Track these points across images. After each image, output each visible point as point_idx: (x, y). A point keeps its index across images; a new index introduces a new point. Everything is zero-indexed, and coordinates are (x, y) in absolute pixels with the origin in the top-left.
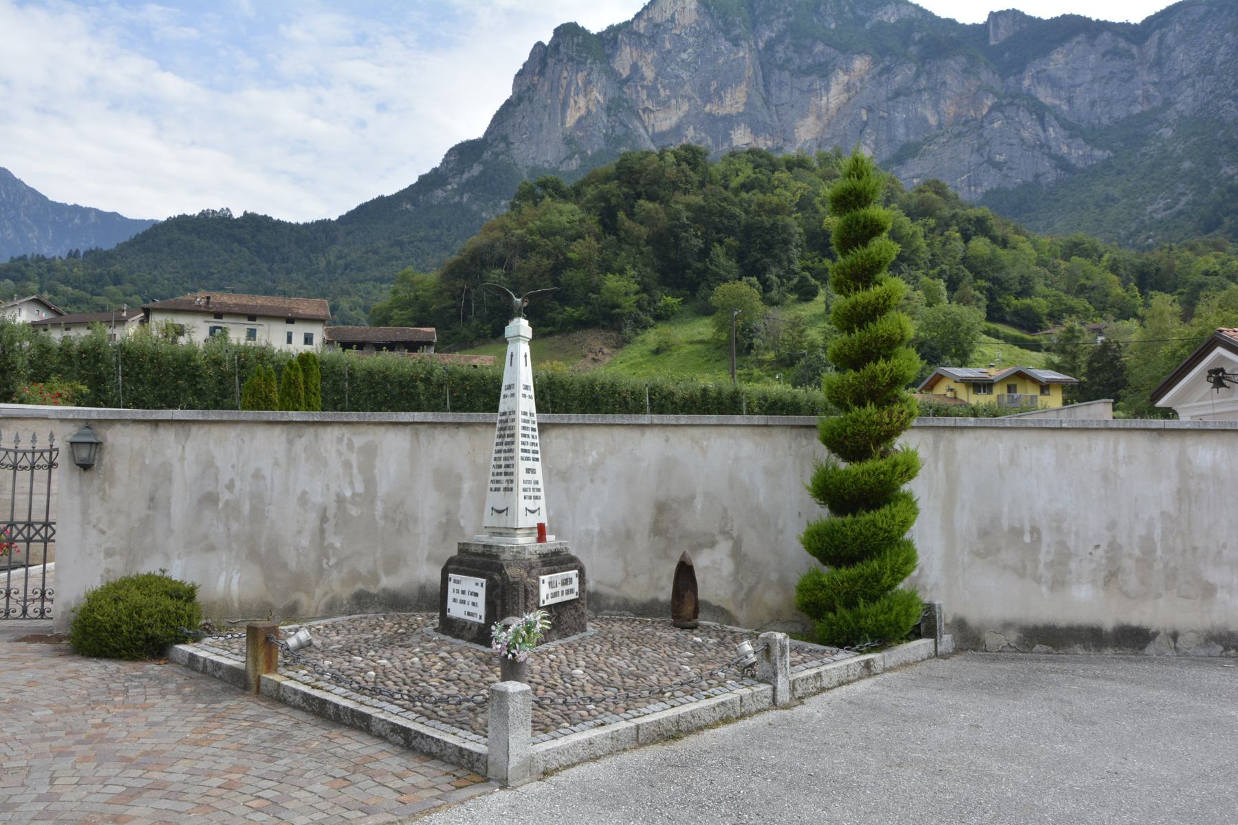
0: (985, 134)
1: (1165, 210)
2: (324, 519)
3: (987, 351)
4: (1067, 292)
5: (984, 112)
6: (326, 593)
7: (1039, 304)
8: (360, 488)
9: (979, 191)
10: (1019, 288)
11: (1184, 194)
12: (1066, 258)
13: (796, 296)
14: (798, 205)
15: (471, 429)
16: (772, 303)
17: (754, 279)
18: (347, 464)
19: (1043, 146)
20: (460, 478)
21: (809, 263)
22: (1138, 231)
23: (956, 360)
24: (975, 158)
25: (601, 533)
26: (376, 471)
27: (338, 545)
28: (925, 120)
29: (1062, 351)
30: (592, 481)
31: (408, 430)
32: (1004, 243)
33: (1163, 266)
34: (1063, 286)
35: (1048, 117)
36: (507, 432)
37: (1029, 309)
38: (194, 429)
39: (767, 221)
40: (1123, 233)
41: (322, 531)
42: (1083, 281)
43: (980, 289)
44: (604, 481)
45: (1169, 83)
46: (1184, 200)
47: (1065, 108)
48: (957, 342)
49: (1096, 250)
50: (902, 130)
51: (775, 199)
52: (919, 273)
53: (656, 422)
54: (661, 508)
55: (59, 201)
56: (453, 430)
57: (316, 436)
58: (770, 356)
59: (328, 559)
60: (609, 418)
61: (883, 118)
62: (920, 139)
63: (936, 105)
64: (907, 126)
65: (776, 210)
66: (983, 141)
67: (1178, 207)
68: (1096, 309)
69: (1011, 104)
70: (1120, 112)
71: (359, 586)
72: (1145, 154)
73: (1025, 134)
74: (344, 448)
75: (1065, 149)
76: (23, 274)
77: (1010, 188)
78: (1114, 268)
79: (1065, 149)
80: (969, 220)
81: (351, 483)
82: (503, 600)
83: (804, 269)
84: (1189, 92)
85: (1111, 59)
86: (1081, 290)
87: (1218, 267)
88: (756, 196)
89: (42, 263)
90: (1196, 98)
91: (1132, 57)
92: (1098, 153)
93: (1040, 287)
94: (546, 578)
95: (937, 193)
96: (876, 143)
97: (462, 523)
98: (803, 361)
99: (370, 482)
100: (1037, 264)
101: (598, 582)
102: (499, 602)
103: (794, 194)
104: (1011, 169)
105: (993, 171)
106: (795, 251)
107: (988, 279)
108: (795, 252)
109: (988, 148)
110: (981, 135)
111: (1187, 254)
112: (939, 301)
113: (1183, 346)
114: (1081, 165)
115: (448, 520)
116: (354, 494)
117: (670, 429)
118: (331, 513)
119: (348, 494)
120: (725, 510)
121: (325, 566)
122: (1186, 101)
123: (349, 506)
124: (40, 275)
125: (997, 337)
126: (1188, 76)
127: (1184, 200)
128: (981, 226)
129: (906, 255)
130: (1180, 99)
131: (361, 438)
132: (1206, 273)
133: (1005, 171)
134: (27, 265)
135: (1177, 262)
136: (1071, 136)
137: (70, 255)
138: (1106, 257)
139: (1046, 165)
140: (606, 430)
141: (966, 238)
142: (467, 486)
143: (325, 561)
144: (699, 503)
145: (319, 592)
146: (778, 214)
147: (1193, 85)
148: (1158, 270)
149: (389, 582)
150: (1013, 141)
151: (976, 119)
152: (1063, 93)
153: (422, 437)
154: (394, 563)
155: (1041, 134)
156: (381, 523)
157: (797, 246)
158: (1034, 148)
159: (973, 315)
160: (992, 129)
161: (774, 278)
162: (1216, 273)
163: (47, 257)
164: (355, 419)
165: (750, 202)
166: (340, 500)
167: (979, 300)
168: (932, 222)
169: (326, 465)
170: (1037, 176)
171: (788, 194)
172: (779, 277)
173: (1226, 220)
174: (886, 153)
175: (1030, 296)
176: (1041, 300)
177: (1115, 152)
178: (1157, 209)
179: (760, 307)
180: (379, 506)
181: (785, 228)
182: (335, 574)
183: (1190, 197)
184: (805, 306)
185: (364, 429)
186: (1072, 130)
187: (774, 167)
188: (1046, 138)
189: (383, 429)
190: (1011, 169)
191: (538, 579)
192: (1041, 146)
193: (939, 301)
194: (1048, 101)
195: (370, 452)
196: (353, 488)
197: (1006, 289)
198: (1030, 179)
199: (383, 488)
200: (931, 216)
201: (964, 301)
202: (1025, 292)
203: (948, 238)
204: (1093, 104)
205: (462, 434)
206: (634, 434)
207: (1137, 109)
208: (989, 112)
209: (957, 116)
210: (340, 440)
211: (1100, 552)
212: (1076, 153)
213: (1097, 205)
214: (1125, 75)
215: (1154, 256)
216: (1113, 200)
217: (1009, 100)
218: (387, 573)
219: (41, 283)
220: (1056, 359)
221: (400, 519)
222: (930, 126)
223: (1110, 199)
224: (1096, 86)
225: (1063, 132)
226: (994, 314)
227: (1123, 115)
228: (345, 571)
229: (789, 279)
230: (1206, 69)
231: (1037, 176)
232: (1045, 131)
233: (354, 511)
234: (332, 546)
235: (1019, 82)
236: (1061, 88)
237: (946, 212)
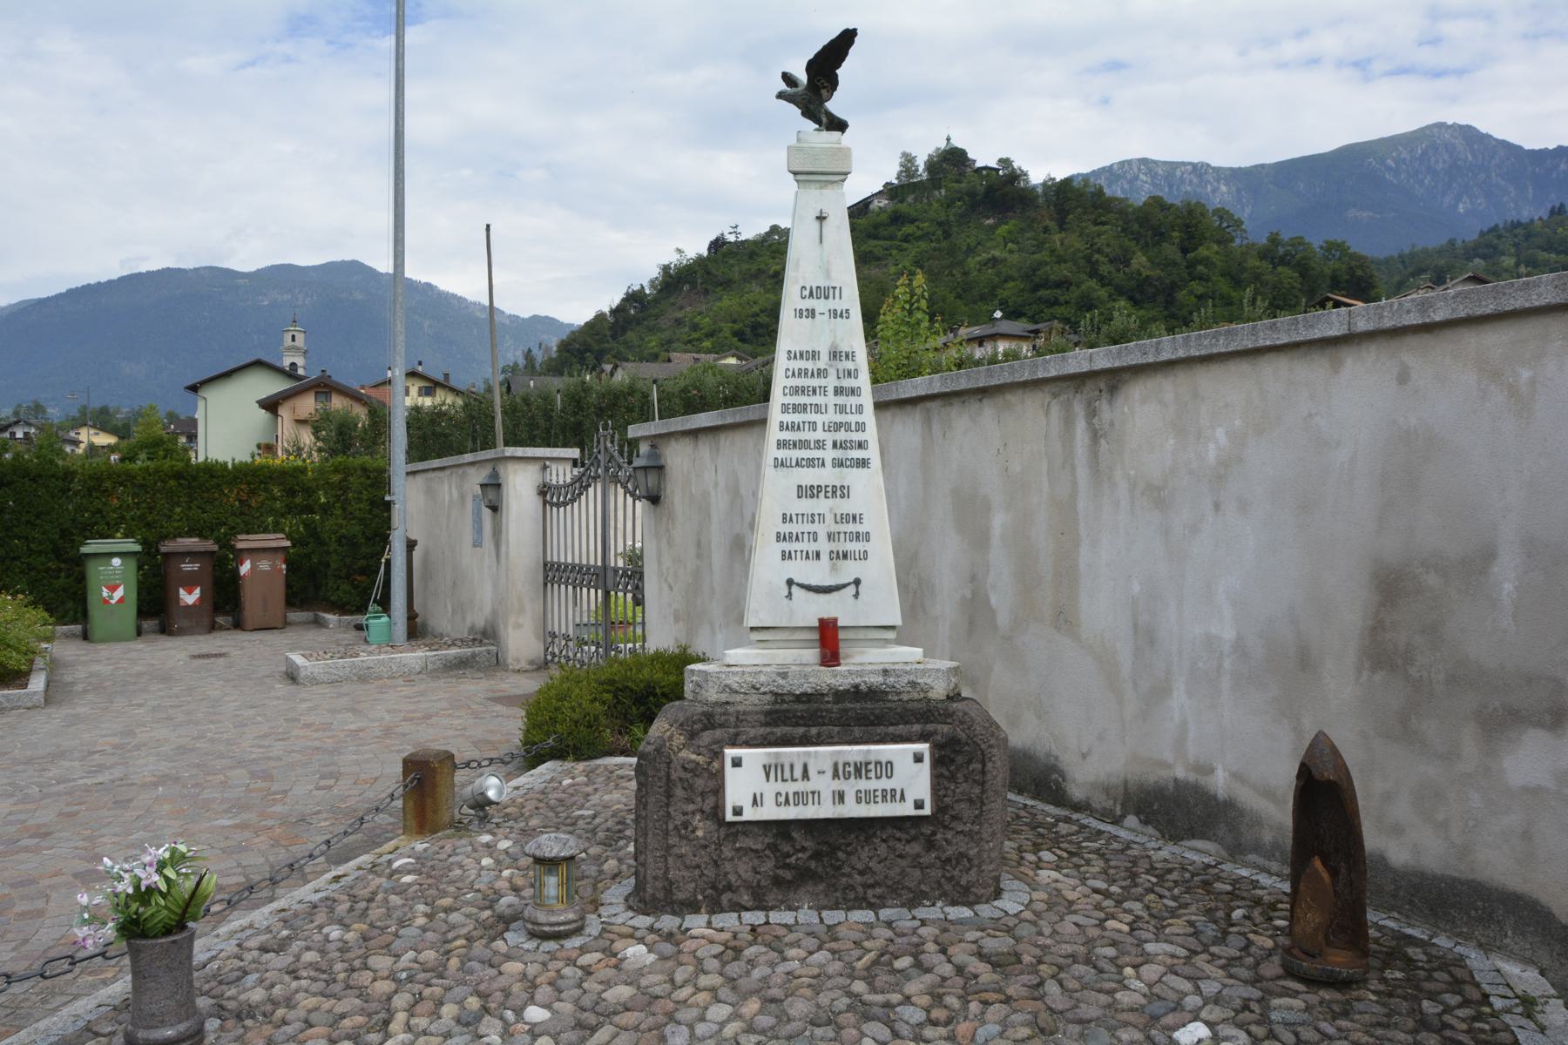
15: (999, 400)
25: (1239, 647)
30: (1217, 506)
38: (725, 440)
44: (1243, 507)
53: (1362, 325)
54: (1390, 586)
55: (1537, 147)
60: (1243, 335)
76: (1495, 248)
89: (1517, 231)
94: (754, 757)
97: (994, 600)
101: (1236, 776)
117: (1412, 341)
124: (1516, 245)
134: (1499, 237)
137: (1552, 212)
140: (1244, 367)
142: (999, 521)
144: (1507, 577)
163: (1523, 221)
191: (718, 755)
206: (1309, 371)
219: (1518, 255)
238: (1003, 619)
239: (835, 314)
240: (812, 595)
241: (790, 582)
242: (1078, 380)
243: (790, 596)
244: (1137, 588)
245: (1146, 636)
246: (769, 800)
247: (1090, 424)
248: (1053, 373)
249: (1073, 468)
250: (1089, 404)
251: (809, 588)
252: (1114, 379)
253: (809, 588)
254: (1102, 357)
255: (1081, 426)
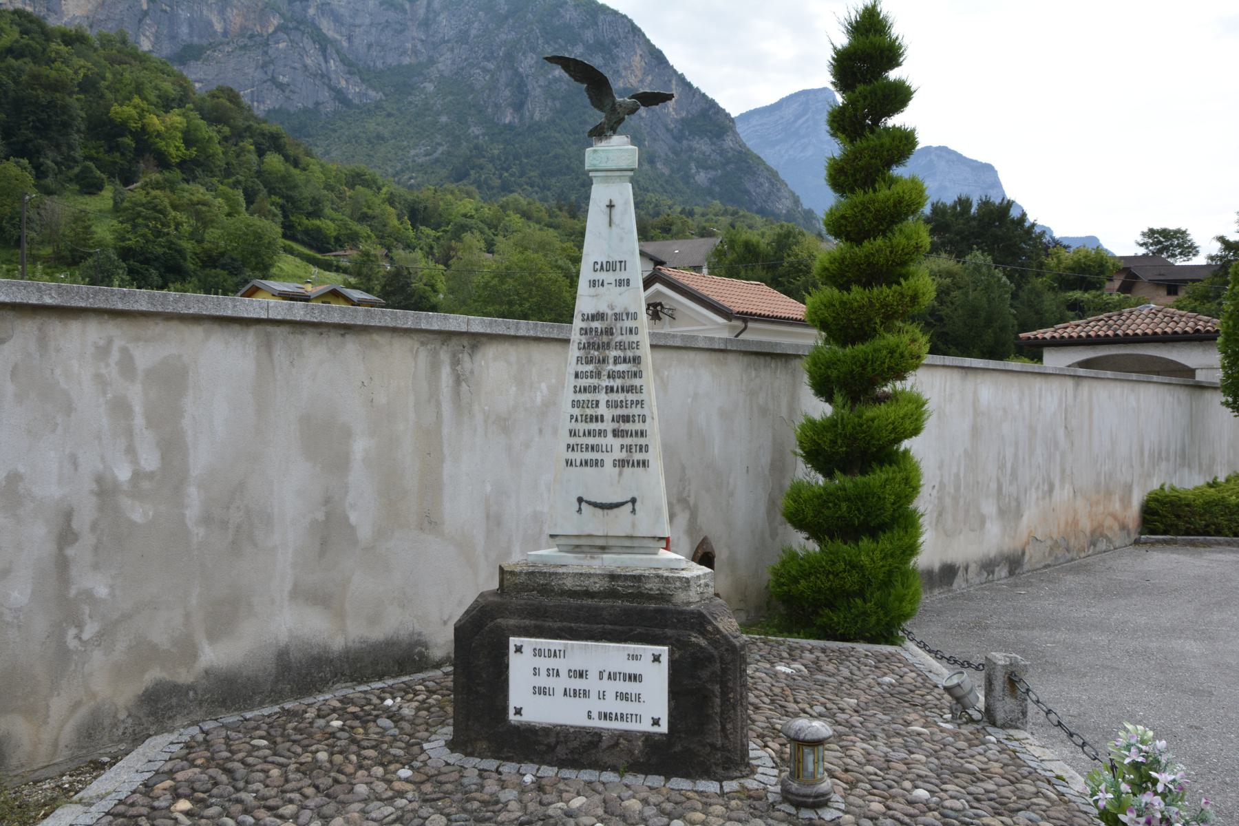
0: (270, 52)
1: (425, 155)
2: (66, 536)
3: (285, 267)
4: (351, 217)
5: (271, 30)
6: (77, 705)
7: (328, 226)
8: (150, 460)
9: (262, 107)
10: (311, 209)
11: (440, 145)
12: (352, 186)
13: (77, 187)
14: (79, 85)
15: (365, 339)
16: (49, 192)
17: (25, 161)
18: (120, 408)
19: (324, 76)
20: (347, 433)
21: (93, 152)
22: (402, 171)
23: (257, 273)
24: (259, 75)
26: (186, 423)
27: (102, 591)
28: (210, 24)
29: (358, 274)
30: (540, 431)
31: (251, 335)
32: (296, 164)
33: (430, 206)
34: (348, 211)
35: (330, 50)
36: (629, 354)
37: (318, 230)
39: (43, 96)
40: (390, 170)
41: (63, 565)
42: (365, 210)
43: (273, 204)
45: (433, 43)
46: (440, 149)
47: (345, 44)
48: (256, 254)
49: (375, 182)
50: (185, 30)
51: (53, 74)
52: (215, 180)
56: (334, 339)
57: (43, 342)
58: (47, 251)
59: (80, 626)
61: (165, 11)
62: (204, 42)
63: (222, 12)
64: (190, 25)
65: (56, 86)
66: (267, 59)
67: (436, 155)
68: (377, 237)
69: (297, 29)
70: (392, 60)
71: (154, 675)
72: (411, 103)
73: (308, 61)
74: (111, 370)
75: (343, 84)
77: (292, 110)
78: (391, 200)
79: (343, 84)
80: (263, 135)
81: (131, 451)
82: (724, 685)
83: (87, 158)
84: (449, 55)
85: (387, 9)
86: (364, 218)
87: (473, 212)
88: (28, 66)
90: (453, 62)
91: (405, 11)
92: (372, 93)
93: (328, 211)
95: (230, 101)
96: (157, 36)
97: (353, 518)
98: (90, 261)
99: (173, 447)
100: (325, 188)
102: (717, 688)
103: (76, 73)
104: (293, 92)
105: (276, 91)
106: (76, 136)
107: (282, 197)
108: (76, 138)
109: (272, 67)
110: (266, 53)
111: (449, 197)
112: (239, 213)
113: (493, 278)
114: (356, 101)
115: (328, 515)
116: (137, 475)
118: (83, 520)
119: (123, 474)
120: (683, 468)
121: (72, 643)
122: (445, 63)
123: (125, 502)
125: (292, 254)
126: (448, 41)
127: (440, 149)
128: (274, 143)
129: (201, 159)
130: (442, 59)
131: (153, 349)
132: (465, 216)
133: (287, 93)
135: (441, 203)
136: (349, 73)
138: (384, 190)
139: (325, 95)
141: (261, 153)
142: (360, 446)
143: (72, 632)
145: (58, 706)
146: (56, 90)
147: (452, 50)
148: (426, 208)
149: (216, 655)
150: (296, 65)
151: (261, 36)
152: (343, 30)
153: (279, 352)
154: (225, 614)
155: (323, 65)
156: (198, 532)
157: (79, 131)
158: (315, 76)
159: (273, 229)
160: (277, 49)
161: (49, 162)
162: (472, 217)
164: (143, 306)
165: (20, 71)
166: (105, 490)
167: (275, 215)
168: (226, 130)
169: (69, 409)
170: (317, 104)
171: (70, 72)
172: (56, 163)
173: (472, 172)
174: (167, 49)
175: (319, 217)
176: (329, 223)
177: (386, 95)
178: (418, 153)
179: (34, 194)
180: (194, 495)
181: (65, 109)
182: (97, 655)
183: (445, 148)
184: (87, 199)
185: (158, 328)
186: (351, 67)
187: (47, 35)
188: (327, 68)
189: (198, 331)
190: (293, 92)
192: (323, 76)
193: (239, 213)
194: (330, 34)
195: (171, 381)
196: (135, 461)
197: (298, 208)
198: (311, 106)
199: (200, 458)
200: (226, 123)
201: (263, 213)
202: (316, 213)
203: (243, 149)
204: (370, 46)
205: (351, 347)
207: (406, 61)
208: (275, 32)
209: (244, 28)
210: (103, 352)
211: (935, 491)
212: (353, 89)
213: (369, 141)
214: (398, 27)
215: (425, 194)
216: (383, 139)
217: (295, 24)
218: (213, 637)
220: (352, 280)
221: (238, 524)
222: (215, 32)
223: (380, 138)
224: (373, 30)
225: (342, 67)
226: (289, 231)
227: (395, 64)
228: (121, 646)
229: (70, 168)
230: (463, 38)
231: (317, 104)
232: (326, 62)
233: (138, 513)
234: (88, 596)
235: (305, 9)
236: (343, 24)
237: (240, 123)
238: (365, 532)
239: (620, 283)
240: (599, 512)
241: (580, 500)
242: (447, 336)
243: (580, 510)
244: (489, 488)
245: (494, 520)
246: (610, 696)
247: (454, 370)
248: (435, 327)
249: (438, 404)
250: (454, 355)
251: (595, 505)
252: (476, 340)
253: (595, 505)
254: (477, 324)
255: (446, 372)
